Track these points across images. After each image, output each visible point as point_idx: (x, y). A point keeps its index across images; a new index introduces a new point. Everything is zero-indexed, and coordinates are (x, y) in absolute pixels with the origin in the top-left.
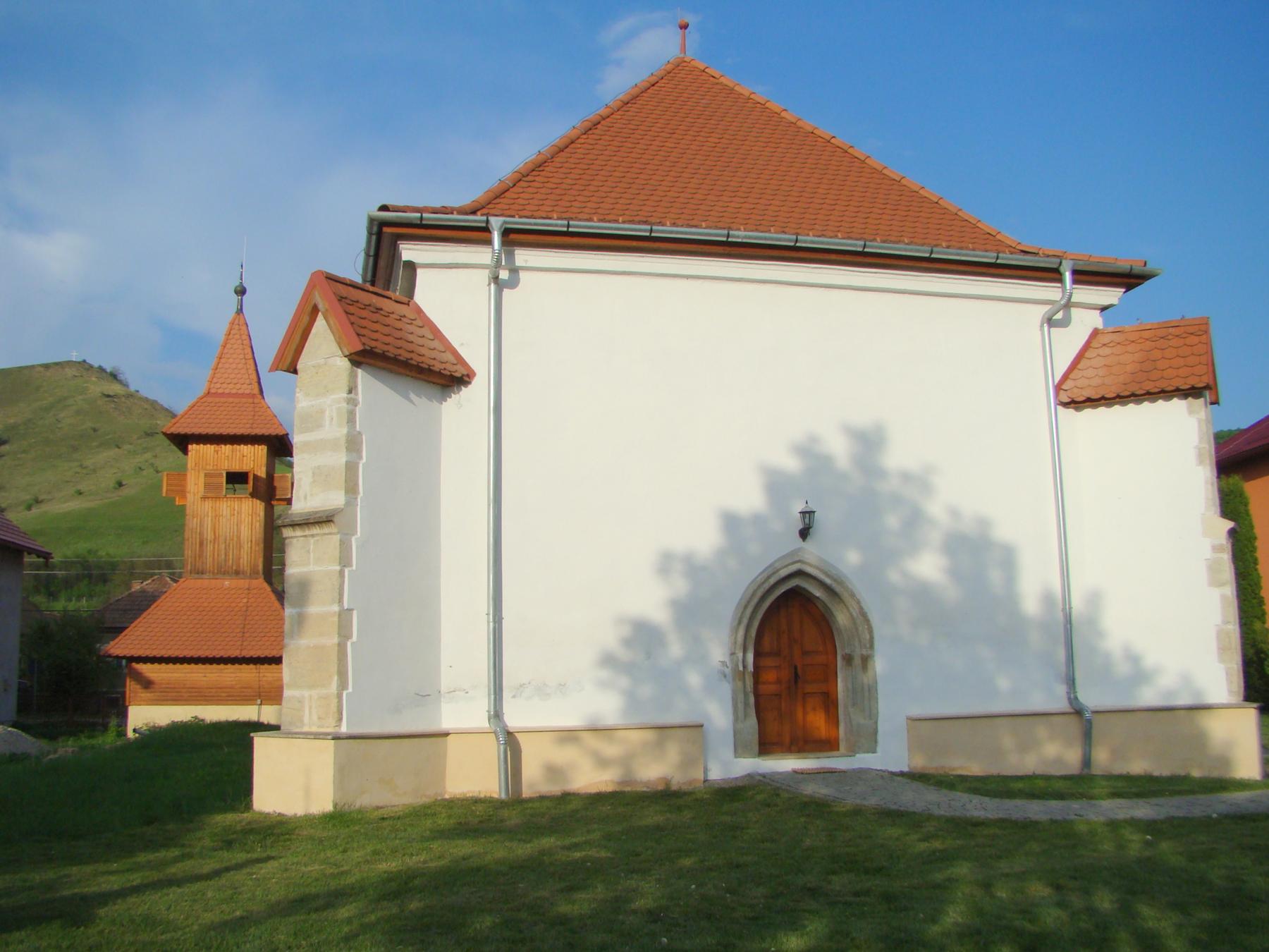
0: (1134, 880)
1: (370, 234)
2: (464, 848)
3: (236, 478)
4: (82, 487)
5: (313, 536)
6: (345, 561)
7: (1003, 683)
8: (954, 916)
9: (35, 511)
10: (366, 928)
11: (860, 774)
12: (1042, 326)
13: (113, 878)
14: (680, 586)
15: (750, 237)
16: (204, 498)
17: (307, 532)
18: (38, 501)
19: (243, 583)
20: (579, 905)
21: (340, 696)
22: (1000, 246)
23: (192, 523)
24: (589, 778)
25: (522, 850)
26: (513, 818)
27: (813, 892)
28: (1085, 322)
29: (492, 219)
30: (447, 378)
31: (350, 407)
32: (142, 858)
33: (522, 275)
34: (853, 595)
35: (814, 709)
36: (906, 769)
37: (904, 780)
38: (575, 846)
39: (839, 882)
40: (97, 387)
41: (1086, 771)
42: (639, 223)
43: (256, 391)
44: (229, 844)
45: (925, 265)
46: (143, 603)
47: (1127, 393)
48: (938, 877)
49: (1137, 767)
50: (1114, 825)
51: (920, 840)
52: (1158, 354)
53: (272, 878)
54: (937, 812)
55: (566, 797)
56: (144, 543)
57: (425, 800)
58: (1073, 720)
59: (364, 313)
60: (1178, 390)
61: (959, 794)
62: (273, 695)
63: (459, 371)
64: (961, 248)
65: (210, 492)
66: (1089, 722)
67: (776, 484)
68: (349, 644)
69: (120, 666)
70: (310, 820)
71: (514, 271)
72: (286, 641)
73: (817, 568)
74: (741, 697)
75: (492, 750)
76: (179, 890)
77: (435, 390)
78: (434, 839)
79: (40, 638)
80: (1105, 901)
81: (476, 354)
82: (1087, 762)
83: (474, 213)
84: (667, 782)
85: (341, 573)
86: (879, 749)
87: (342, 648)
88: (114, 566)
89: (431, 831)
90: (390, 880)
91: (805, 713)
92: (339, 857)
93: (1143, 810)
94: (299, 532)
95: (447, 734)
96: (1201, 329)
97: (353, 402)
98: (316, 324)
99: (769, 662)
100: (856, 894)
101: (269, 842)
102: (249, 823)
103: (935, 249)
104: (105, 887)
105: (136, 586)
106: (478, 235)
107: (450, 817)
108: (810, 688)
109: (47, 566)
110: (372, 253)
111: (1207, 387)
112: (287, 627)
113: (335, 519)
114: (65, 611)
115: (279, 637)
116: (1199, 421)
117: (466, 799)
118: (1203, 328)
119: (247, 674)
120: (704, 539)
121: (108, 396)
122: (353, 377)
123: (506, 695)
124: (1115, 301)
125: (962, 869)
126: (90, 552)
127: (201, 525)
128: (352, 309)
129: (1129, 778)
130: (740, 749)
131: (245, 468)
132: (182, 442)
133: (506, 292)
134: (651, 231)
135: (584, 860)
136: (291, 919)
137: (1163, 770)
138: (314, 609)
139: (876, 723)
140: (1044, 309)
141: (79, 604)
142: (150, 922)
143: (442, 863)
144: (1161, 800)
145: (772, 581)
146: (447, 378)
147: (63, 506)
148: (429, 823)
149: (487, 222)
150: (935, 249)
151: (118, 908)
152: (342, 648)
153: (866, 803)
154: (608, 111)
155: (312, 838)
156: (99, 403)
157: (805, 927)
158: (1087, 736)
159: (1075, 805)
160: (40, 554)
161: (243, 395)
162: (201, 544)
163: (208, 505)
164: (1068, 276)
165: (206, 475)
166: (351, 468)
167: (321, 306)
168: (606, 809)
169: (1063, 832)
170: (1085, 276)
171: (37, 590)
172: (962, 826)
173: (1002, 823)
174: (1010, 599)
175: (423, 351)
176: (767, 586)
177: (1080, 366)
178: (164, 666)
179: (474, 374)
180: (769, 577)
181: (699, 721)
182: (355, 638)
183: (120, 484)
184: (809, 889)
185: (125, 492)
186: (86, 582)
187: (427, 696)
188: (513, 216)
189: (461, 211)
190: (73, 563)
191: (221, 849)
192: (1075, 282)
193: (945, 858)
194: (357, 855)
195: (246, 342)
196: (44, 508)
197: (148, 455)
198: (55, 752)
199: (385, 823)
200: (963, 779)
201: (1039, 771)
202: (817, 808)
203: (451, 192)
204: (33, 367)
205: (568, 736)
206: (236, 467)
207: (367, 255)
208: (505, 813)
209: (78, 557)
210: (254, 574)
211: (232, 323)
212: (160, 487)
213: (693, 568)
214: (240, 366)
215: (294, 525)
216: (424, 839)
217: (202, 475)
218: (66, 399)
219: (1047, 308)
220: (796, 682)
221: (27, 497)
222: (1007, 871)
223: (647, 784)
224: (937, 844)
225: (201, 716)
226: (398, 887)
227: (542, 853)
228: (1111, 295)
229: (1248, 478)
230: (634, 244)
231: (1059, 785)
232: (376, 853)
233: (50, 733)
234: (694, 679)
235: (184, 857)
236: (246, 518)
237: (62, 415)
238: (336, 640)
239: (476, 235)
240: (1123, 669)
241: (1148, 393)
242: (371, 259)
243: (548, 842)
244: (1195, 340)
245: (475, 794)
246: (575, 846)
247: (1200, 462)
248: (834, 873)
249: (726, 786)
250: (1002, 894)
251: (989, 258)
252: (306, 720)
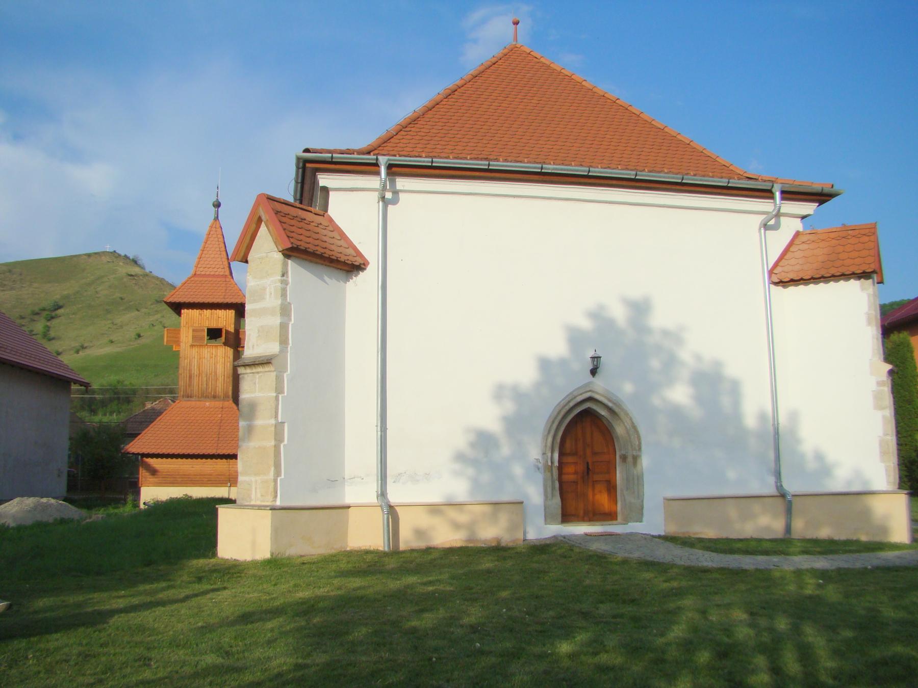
0: (804, 609)
1: (298, 168)
2: (356, 582)
3: (214, 334)
4: (113, 338)
5: (258, 373)
6: (279, 390)
7: (731, 474)
8: (678, 632)
9: (82, 354)
10: (286, 633)
11: (631, 536)
12: (760, 229)
13: (120, 601)
14: (509, 407)
15: (562, 170)
16: (192, 346)
17: (254, 370)
18: (83, 347)
19: (219, 404)
20: (428, 620)
21: (275, 481)
22: (731, 173)
23: (184, 363)
24: (445, 536)
25: (394, 585)
26: (392, 564)
27: (585, 615)
28: (790, 227)
29: (380, 158)
30: (351, 266)
31: (284, 286)
32: (141, 588)
33: (401, 195)
34: (627, 414)
35: (600, 492)
36: (663, 533)
37: (661, 541)
38: (430, 583)
39: (604, 609)
40: (124, 269)
41: (788, 536)
42: (481, 159)
43: (228, 273)
44: (200, 579)
45: (678, 187)
46: (151, 417)
47: (787, 280)
48: (671, 606)
49: (824, 533)
50: (799, 573)
51: (665, 581)
52: (840, 249)
53: (227, 601)
54: (679, 562)
55: (429, 550)
56: (155, 376)
57: (333, 552)
58: (779, 501)
59: (293, 222)
60: (853, 274)
61: (697, 551)
62: (231, 480)
63: (358, 261)
64: (704, 176)
65: (196, 342)
66: (790, 502)
67: (575, 338)
68: (282, 446)
69: (137, 459)
70: (255, 564)
71: (396, 193)
72: (240, 443)
73: (603, 396)
74: (549, 483)
75: (379, 518)
76: (163, 609)
77: (342, 274)
78: (336, 577)
79: (83, 441)
80: (782, 624)
81: (369, 249)
82: (788, 529)
83: (369, 153)
84: (499, 541)
85: (277, 398)
86: (644, 519)
87: (277, 448)
88: (134, 392)
89: (335, 571)
90: (303, 603)
91: (594, 495)
92: (272, 588)
93: (821, 563)
94: (248, 370)
95: (349, 507)
96: (871, 231)
97: (285, 283)
98: (261, 229)
99: (570, 459)
100: (614, 617)
101: (226, 578)
102: (214, 566)
103: (685, 177)
104: (115, 606)
105: (149, 406)
106: (370, 168)
107: (348, 562)
108: (596, 477)
109: (87, 392)
110: (300, 181)
111: (874, 272)
112: (241, 433)
113: (273, 361)
114: (100, 422)
115: (235, 440)
116: (869, 295)
117: (361, 551)
118: (873, 230)
119: (221, 465)
120: (526, 375)
121: (131, 275)
122: (285, 266)
123: (389, 480)
124: (811, 212)
125: (688, 602)
126: (118, 382)
128: (284, 219)
129: (816, 542)
130: (548, 518)
131: (220, 326)
132: (177, 307)
133: (390, 207)
134: (489, 165)
135: (434, 592)
136: (234, 628)
137: (841, 536)
138: (259, 422)
139: (643, 501)
140: (763, 217)
141: (111, 418)
142: (141, 629)
143: (339, 592)
144: (836, 557)
145: (572, 404)
146: (351, 266)
147: (101, 350)
148: (334, 566)
149: (377, 159)
150: (685, 177)
151: (115, 620)
152: (277, 448)
153: (631, 556)
154: (463, 82)
155: (255, 576)
156: (125, 280)
157: (574, 637)
158: (789, 511)
159: (775, 559)
160: (82, 384)
161: (218, 276)
162: (190, 377)
163: (195, 350)
164: (778, 195)
165: (194, 330)
166: (284, 327)
167: (263, 218)
168: (455, 558)
169: (764, 577)
170: (790, 195)
171: (82, 408)
172: (693, 572)
173: (721, 570)
174: (736, 415)
175: (333, 247)
176: (567, 408)
177: (786, 257)
179: (368, 263)
180: (569, 402)
181: (519, 499)
182: (286, 442)
183: (139, 336)
184: (583, 613)
186: (116, 402)
187: (335, 481)
188: (395, 156)
189: (360, 152)
190: (108, 390)
191: (194, 582)
192: (782, 199)
193: (679, 593)
194: (283, 587)
195: (221, 240)
196: (88, 352)
197: (159, 316)
198: (90, 518)
199: (304, 567)
200: (701, 540)
201: (755, 536)
202: (599, 559)
203: (355, 138)
205: (434, 509)
206: (214, 325)
207: (297, 182)
208: (386, 559)
209: (110, 385)
210: (226, 397)
211: (211, 227)
212: (162, 337)
213: (518, 395)
215: (245, 366)
216: (330, 577)
217: (191, 331)
219: (764, 217)
220: (588, 473)
221: (76, 344)
222: (719, 603)
223: (485, 541)
224: (675, 584)
225: (190, 494)
226: (307, 609)
227: (407, 587)
228: (808, 208)
229: (913, 335)
230: (477, 174)
231: (768, 545)
232: (295, 586)
233: (88, 505)
234: (518, 470)
235: (169, 587)
236: (220, 360)
237: (100, 288)
238: (273, 443)
239: (369, 168)
240: (811, 465)
241: (833, 276)
242: (299, 185)
243: (411, 579)
244: (866, 239)
245: (367, 548)
246: (430, 583)
247: (869, 323)
248: (602, 602)
249: (538, 543)
250: (714, 618)
251: (723, 182)
252: (253, 496)
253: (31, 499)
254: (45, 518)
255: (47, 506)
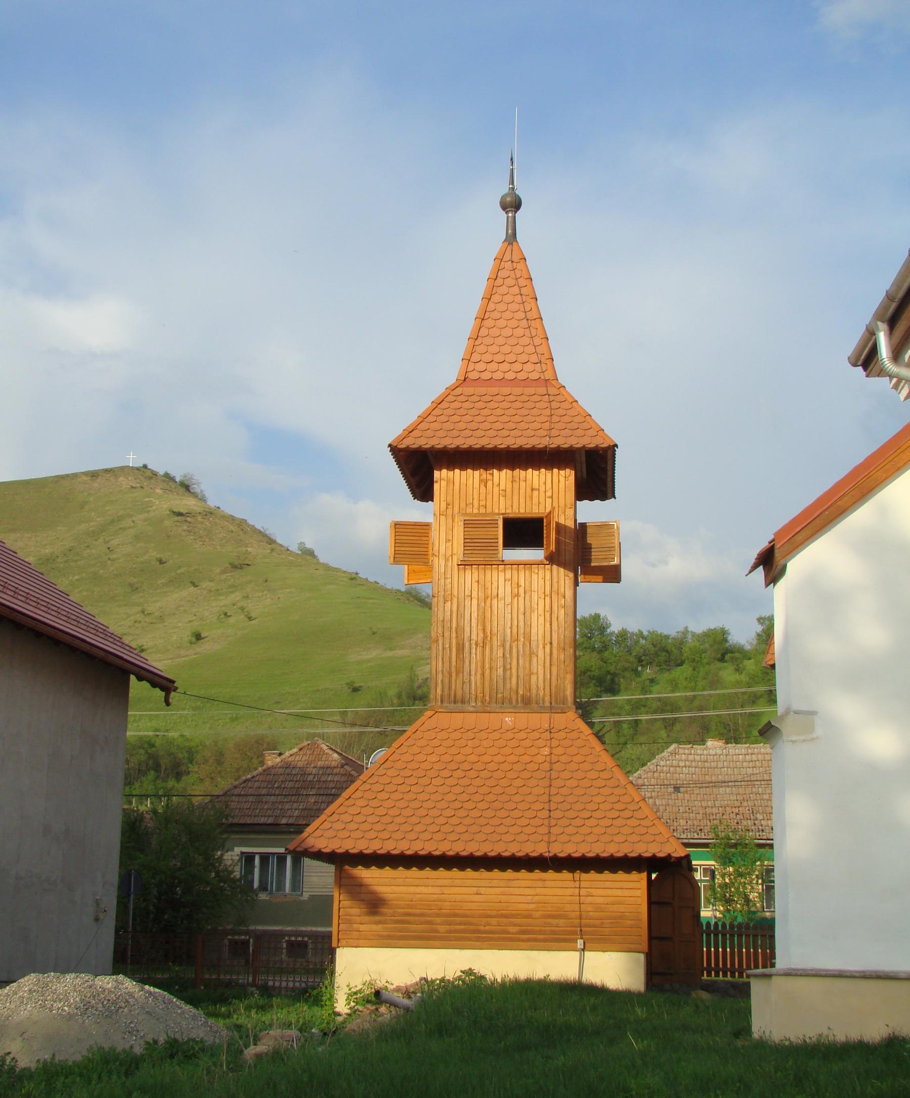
3: (523, 531)
16: (464, 565)
19: (541, 720)
23: (443, 611)
40: (164, 503)
65: (476, 556)
121: (180, 514)
127: (460, 615)
156: (167, 523)
162: (461, 648)
163: (470, 577)
165: (467, 524)
178: (401, 872)
183: (198, 637)
185: (204, 647)
197: (237, 596)
204: (75, 475)
206: (522, 509)
211: (499, 259)
214: (519, 332)
218: (120, 519)
237: (115, 542)
253: (70, 977)
254: (122, 1043)
255: (111, 1009)
